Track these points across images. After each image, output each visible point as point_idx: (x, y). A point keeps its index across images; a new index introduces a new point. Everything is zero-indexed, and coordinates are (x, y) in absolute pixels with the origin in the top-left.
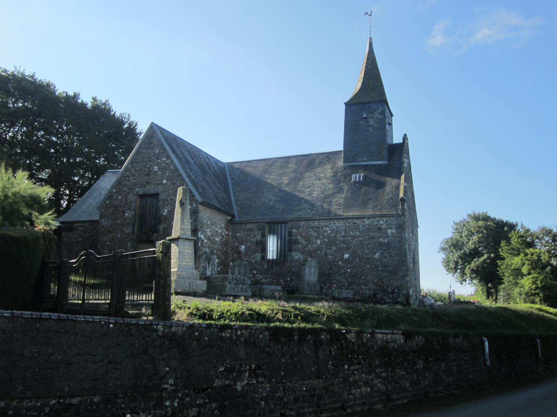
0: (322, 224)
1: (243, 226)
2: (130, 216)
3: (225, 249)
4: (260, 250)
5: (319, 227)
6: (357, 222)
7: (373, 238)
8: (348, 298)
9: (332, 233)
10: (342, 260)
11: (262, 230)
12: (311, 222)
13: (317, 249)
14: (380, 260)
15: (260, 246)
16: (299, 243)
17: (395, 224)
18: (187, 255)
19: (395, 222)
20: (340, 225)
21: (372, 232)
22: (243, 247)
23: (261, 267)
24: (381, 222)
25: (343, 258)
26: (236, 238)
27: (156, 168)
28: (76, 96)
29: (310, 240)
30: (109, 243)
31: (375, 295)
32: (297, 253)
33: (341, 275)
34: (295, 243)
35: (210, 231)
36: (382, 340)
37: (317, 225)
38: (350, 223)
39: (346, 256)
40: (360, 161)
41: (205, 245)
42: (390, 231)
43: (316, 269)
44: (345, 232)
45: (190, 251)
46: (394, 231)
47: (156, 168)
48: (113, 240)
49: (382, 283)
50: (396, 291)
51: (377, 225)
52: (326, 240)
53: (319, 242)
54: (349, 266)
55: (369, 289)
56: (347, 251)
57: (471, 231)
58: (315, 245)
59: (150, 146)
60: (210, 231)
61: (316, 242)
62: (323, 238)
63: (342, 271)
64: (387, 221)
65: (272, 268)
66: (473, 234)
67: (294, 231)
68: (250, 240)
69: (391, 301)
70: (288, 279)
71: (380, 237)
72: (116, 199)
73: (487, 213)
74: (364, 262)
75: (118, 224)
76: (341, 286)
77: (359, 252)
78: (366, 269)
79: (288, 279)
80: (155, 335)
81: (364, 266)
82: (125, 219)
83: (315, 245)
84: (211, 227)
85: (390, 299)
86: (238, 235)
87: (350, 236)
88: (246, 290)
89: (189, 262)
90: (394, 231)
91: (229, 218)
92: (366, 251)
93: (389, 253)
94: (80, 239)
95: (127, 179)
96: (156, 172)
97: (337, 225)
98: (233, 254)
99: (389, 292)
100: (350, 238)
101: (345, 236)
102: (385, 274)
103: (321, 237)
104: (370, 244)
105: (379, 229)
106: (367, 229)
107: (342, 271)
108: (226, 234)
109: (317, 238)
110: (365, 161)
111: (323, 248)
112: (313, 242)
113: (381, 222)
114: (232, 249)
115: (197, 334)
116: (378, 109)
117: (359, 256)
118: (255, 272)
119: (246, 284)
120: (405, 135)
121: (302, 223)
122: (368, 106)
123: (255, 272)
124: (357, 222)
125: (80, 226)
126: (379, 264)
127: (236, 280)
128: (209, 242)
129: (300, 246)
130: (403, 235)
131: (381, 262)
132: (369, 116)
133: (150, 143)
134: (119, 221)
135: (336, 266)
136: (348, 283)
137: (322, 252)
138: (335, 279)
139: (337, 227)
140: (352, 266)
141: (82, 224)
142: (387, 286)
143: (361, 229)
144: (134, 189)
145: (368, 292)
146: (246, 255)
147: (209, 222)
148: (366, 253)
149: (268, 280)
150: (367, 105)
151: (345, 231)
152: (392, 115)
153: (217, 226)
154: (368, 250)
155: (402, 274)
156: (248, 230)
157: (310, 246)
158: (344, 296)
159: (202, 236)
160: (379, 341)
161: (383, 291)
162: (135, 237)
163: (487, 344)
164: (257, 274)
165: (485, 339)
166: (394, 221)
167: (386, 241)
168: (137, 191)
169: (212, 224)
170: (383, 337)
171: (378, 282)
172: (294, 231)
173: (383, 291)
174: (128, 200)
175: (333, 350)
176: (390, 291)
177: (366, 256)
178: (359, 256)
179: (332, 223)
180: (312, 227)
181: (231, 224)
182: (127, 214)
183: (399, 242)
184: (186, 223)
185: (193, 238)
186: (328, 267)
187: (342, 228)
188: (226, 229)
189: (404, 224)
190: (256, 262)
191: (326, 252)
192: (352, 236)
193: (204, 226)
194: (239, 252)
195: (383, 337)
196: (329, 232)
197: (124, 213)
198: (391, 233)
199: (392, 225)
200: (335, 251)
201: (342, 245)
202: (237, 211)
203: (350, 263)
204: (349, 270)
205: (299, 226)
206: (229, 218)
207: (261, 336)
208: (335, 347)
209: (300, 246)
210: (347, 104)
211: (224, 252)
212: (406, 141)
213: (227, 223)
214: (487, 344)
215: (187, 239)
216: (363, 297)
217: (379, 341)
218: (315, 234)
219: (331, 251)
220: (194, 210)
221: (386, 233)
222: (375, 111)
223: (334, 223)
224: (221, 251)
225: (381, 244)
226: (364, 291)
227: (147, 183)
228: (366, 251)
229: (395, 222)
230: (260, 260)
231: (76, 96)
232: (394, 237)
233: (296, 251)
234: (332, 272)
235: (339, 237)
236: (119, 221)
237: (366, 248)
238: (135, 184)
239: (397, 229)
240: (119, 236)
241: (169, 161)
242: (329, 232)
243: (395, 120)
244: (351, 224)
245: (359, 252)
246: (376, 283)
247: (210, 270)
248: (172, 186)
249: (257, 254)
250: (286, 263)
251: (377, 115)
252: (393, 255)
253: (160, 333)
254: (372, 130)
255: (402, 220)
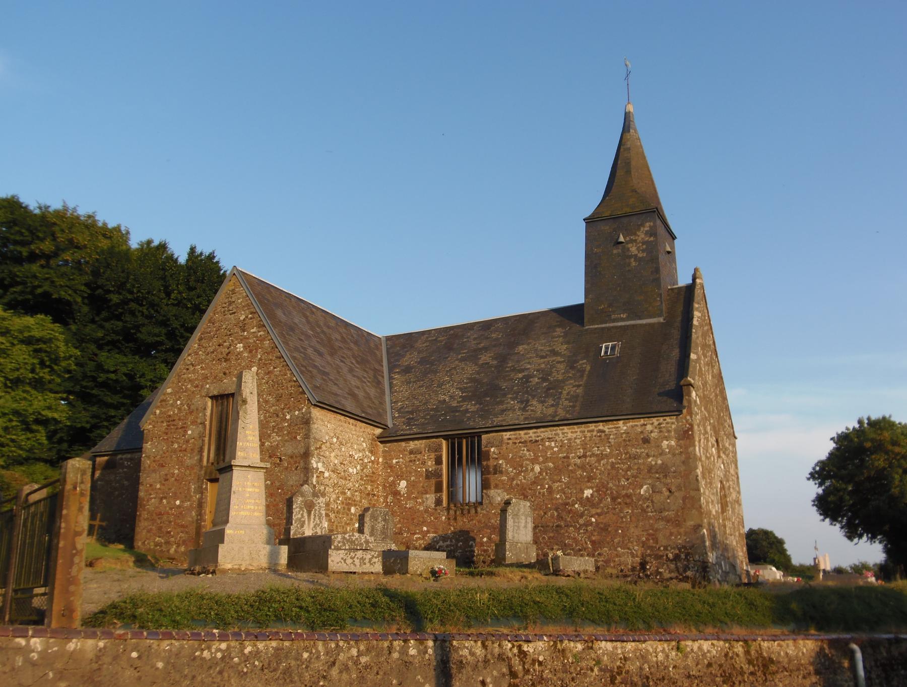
0: (542, 435)
1: (403, 444)
2: (196, 435)
3: (369, 488)
4: (433, 488)
5: (536, 441)
6: (606, 429)
7: (636, 457)
8: (585, 571)
9: (560, 451)
10: (581, 501)
11: (436, 451)
12: (522, 432)
13: (534, 482)
14: (649, 499)
15: (433, 481)
16: (501, 472)
17: (675, 430)
18: (249, 498)
19: (673, 426)
20: (574, 435)
21: (633, 446)
22: (403, 484)
23: (436, 518)
24: (649, 428)
25: (582, 498)
26: (391, 467)
27: (240, 346)
28: (163, 247)
29: (522, 466)
30: (158, 486)
31: (643, 565)
32: (499, 491)
33: (579, 529)
34: (495, 473)
35: (336, 456)
36: (612, 655)
37: (534, 439)
38: (593, 431)
39: (588, 493)
40: (614, 321)
41: (326, 482)
42: (665, 442)
43: (529, 520)
44: (584, 449)
45: (257, 490)
46: (673, 443)
47: (240, 346)
48: (166, 480)
49: (656, 541)
50: (683, 556)
51: (642, 432)
52: (551, 464)
53: (537, 468)
54: (593, 511)
55: (632, 554)
56: (589, 484)
57: (203, 278)
58: (531, 474)
59: (231, 308)
60: (336, 456)
61: (532, 470)
62: (544, 462)
63: (581, 521)
64: (659, 424)
65: (455, 519)
66: (203, 282)
67: (492, 450)
68: (416, 471)
69: (673, 575)
70: (485, 539)
71: (648, 456)
72: (172, 405)
73: (890, 416)
74: (620, 503)
75: (175, 451)
76: (580, 550)
77: (611, 485)
78: (625, 517)
79: (485, 539)
80: (19, 661)
81: (621, 511)
82: (188, 441)
83: (531, 474)
84: (340, 450)
85: (670, 572)
86: (394, 461)
87: (593, 455)
88: (370, 560)
89: (254, 511)
90: (673, 443)
91: (378, 431)
92: (623, 482)
93: (666, 484)
94: (126, 483)
95: (192, 368)
96: (240, 353)
97: (570, 435)
98: (386, 497)
99: (668, 559)
100: (593, 459)
101: (585, 456)
102: (661, 525)
103: (541, 459)
104: (629, 468)
105: (646, 441)
106: (624, 440)
107: (581, 521)
108: (373, 462)
109: (534, 461)
110: (623, 320)
111: (544, 479)
112: (527, 469)
113: (649, 428)
114: (384, 487)
115: (134, 655)
116: (642, 225)
117: (612, 493)
118: (425, 529)
119: (371, 550)
120: (696, 270)
121: (506, 435)
122: (626, 220)
123: (425, 529)
124: (606, 429)
125: (126, 459)
126: (648, 506)
127: (352, 542)
128: (334, 476)
129: (505, 478)
130: (691, 449)
131: (652, 502)
132: (628, 239)
133: (231, 303)
134: (176, 446)
135: (570, 512)
136: (593, 542)
137: (543, 487)
138: (569, 537)
139: (569, 440)
140: (599, 511)
141: (129, 456)
142: (666, 548)
143: (612, 441)
144: (202, 386)
145: (630, 560)
146: (409, 498)
147: (335, 440)
148: (624, 486)
149: (449, 543)
150: (625, 220)
151: (584, 445)
152: (674, 237)
153: (352, 447)
154: (628, 479)
155: (692, 523)
156: (411, 452)
157: (521, 477)
158: (577, 569)
159: (320, 465)
160: (605, 658)
161: (658, 557)
162: (203, 472)
163: (859, 655)
164: (428, 532)
165: (855, 647)
166: (673, 423)
167: (660, 462)
168: (208, 389)
169: (341, 443)
170: (615, 648)
171: (647, 539)
172: (492, 450)
173: (658, 557)
174: (192, 407)
175: (489, 680)
176: (671, 556)
177: (624, 492)
178: (612, 493)
179: (559, 432)
180: (525, 442)
181: (381, 442)
182: (189, 432)
183: (683, 462)
184: (250, 438)
185: (262, 465)
186: (556, 514)
187: (578, 441)
188: (371, 452)
189: (691, 428)
190: (426, 511)
191: (550, 487)
192: (597, 455)
193: (323, 447)
194: (396, 493)
195: (615, 648)
196: (556, 449)
197: (184, 428)
198: (669, 446)
199: (669, 431)
200: (568, 485)
201: (579, 472)
202: (393, 418)
203: (593, 506)
204: (593, 520)
205: (502, 441)
206: (378, 431)
207: (306, 655)
208: (495, 673)
209: (505, 478)
210: (589, 221)
211: (368, 494)
212: (698, 281)
213: (373, 440)
214: (859, 655)
215: (249, 466)
216: (622, 571)
217: (605, 658)
218: (529, 455)
219: (559, 484)
220: (303, 418)
221: (659, 446)
222: (639, 229)
223: (563, 433)
224: (361, 491)
225: (650, 469)
226: (622, 559)
227: (225, 374)
228: (623, 482)
229: (673, 426)
230: (433, 506)
231: (163, 247)
232: (674, 455)
233: (496, 486)
234: (562, 524)
235: (573, 458)
236: (176, 446)
237: (624, 477)
238: (206, 378)
239: (678, 439)
240: (176, 471)
241: (262, 333)
242: (556, 449)
243: (680, 247)
244: (595, 433)
245: (611, 485)
246: (643, 543)
247: (312, 525)
248: (266, 377)
249: (428, 496)
250: (479, 509)
251: (641, 236)
252: (673, 489)
253: (35, 656)
254: (634, 264)
255: (687, 421)
